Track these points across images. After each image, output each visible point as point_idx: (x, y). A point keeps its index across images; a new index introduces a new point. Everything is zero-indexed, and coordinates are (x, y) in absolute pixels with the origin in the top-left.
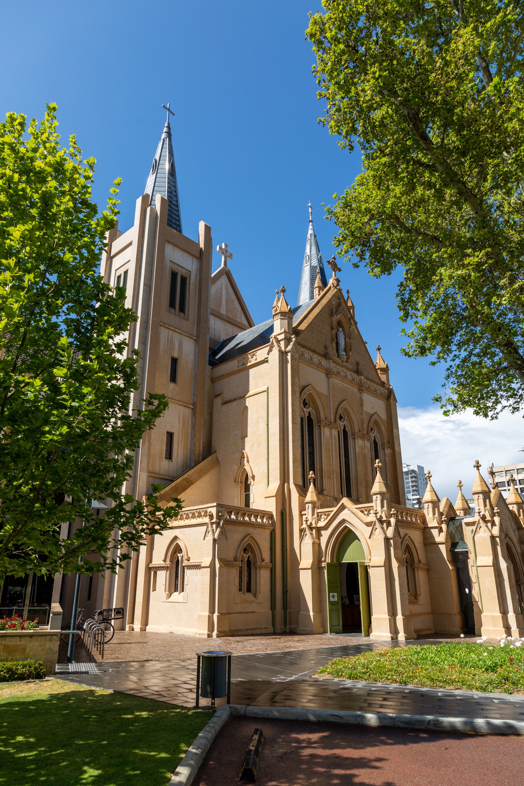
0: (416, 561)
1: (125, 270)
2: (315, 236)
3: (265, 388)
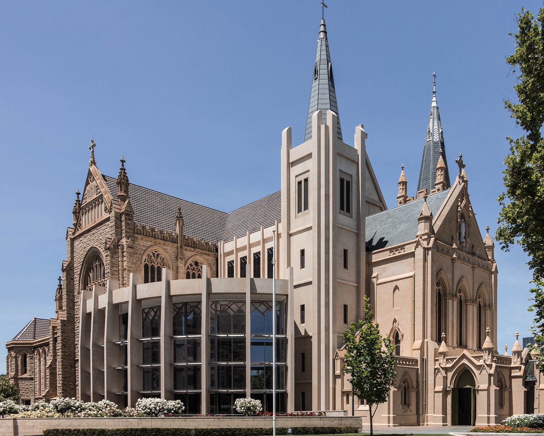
0: (504, 386)
1: (306, 177)
2: (438, 108)
3: (411, 274)
